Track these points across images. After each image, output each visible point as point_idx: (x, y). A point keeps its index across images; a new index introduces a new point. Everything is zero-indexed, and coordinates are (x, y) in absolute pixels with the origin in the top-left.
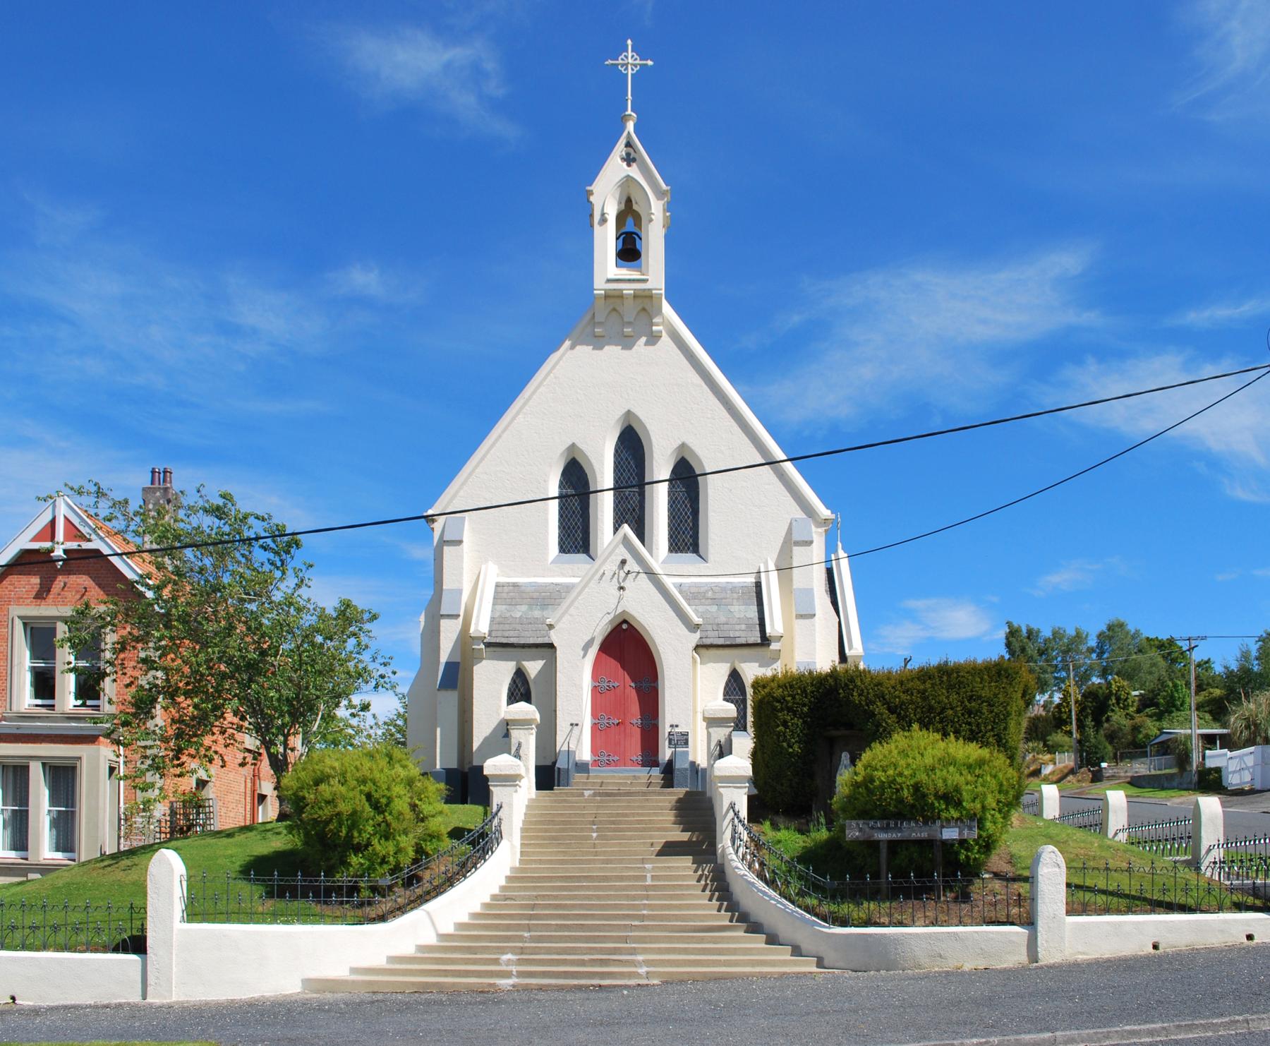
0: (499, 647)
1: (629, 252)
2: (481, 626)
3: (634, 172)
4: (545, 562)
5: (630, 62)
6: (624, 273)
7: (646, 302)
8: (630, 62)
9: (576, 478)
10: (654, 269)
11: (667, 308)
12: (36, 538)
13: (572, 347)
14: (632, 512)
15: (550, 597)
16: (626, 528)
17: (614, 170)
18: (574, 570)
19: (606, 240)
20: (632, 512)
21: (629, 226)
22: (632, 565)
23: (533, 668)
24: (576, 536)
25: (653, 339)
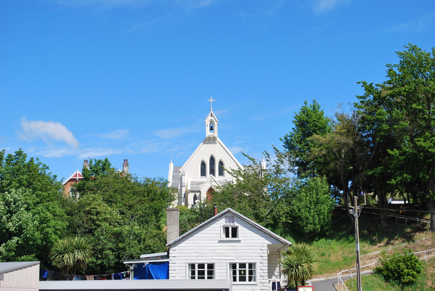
0: (192, 191)
1: (212, 129)
2: (189, 188)
3: (212, 118)
4: (198, 178)
5: (211, 100)
6: (212, 134)
7: (214, 139)
8: (211, 100)
9: (203, 164)
10: (215, 133)
11: (218, 139)
12: (73, 177)
13: (203, 144)
14: (212, 172)
15: (200, 183)
16: (211, 175)
17: (209, 118)
18: (203, 179)
19: (208, 128)
20: (212, 172)
21: (212, 125)
22: (212, 180)
23: (198, 194)
24: (203, 173)
25: (216, 143)
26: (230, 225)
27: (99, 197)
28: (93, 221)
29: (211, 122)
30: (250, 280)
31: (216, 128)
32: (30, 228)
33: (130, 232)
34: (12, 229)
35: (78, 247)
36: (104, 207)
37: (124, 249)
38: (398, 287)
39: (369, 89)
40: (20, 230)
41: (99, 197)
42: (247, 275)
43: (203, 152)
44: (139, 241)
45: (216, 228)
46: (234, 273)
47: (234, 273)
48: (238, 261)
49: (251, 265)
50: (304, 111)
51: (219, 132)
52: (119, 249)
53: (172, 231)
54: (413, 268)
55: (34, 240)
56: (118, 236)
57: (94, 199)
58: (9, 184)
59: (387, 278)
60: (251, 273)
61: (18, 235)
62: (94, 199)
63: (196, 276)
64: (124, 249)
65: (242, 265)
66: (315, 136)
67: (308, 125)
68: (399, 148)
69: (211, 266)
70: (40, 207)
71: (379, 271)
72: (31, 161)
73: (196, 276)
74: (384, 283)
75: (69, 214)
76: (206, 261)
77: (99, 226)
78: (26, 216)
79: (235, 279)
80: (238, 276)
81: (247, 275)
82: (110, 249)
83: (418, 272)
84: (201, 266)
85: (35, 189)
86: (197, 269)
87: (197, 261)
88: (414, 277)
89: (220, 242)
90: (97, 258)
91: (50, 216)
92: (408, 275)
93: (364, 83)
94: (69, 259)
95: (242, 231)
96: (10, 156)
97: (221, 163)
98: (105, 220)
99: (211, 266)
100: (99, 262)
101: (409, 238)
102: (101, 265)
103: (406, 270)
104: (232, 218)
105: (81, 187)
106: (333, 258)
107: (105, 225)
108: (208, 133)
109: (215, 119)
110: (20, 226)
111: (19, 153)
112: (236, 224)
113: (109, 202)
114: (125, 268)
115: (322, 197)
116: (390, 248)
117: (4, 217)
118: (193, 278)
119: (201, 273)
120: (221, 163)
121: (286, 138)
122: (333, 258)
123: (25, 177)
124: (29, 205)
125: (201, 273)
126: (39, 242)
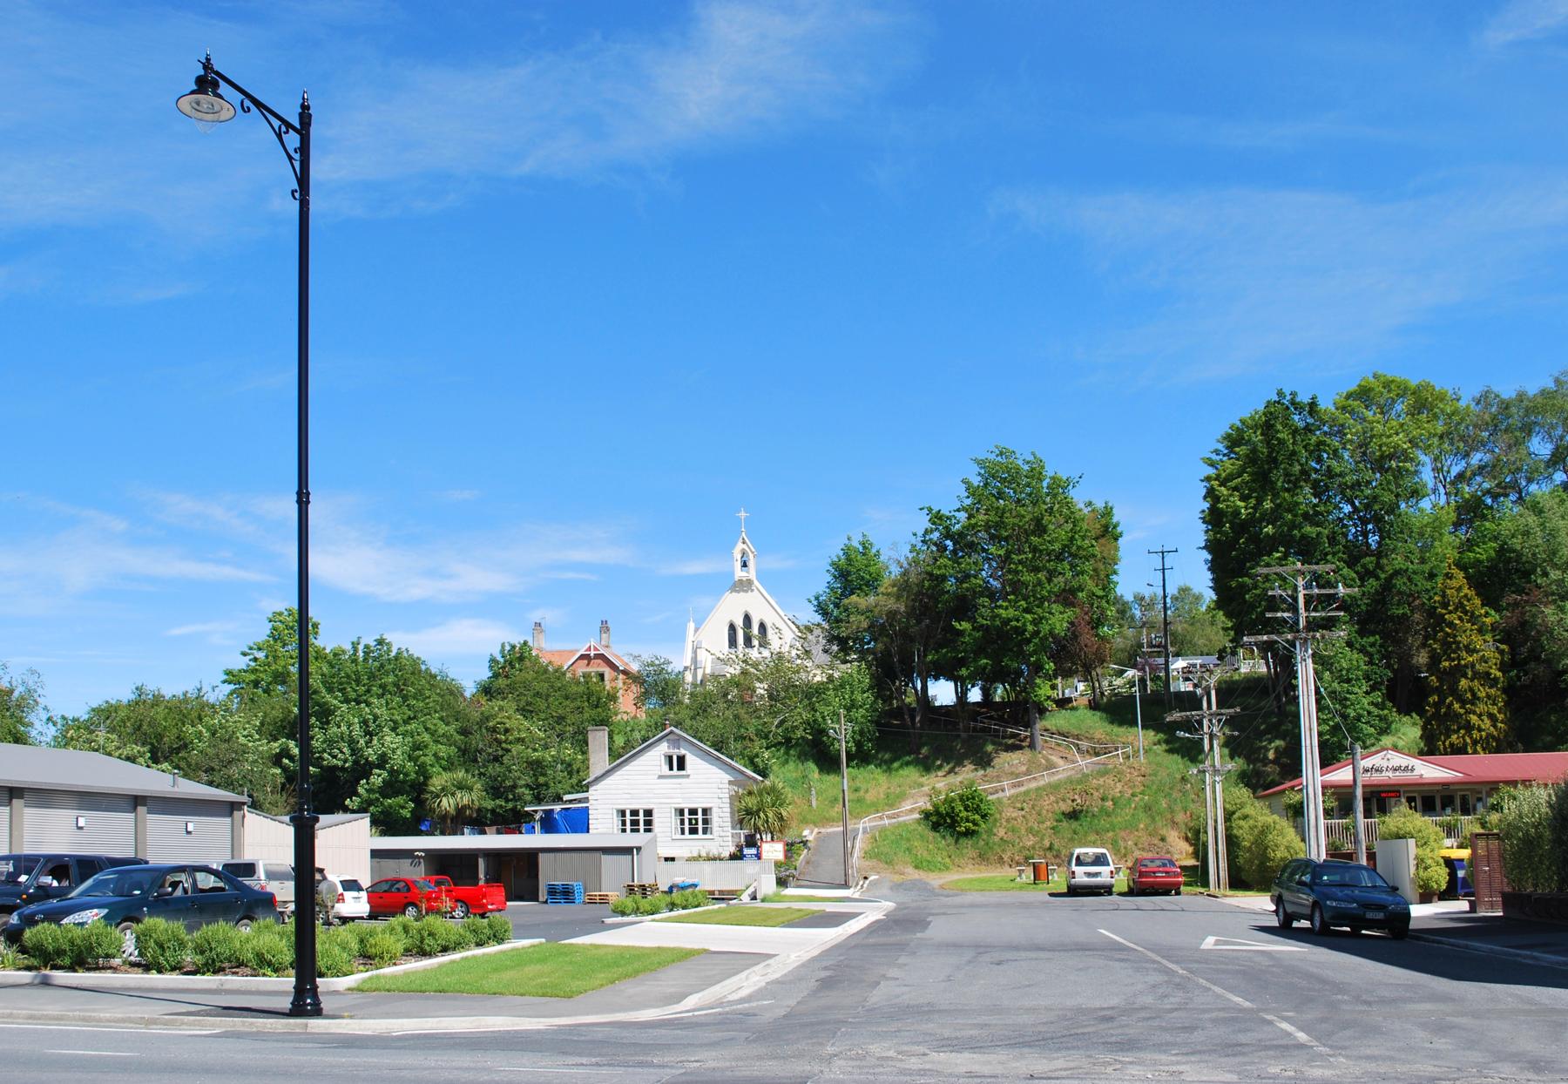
1: (745, 565)
5: (743, 514)
8: (743, 514)
9: (732, 628)
17: (740, 546)
19: (738, 564)
24: (733, 642)
26: (675, 752)
27: (510, 705)
28: (499, 742)
29: (744, 553)
30: (705, 831)
31: (751, 564)
32: (398, 759)
33: (556, 760)
34: (373, 758)
35: (461, 786)
36: (517, 722)
37: (546, 785)
38: (950, 840)
39: (937, 518)
40: (383, 761)
41: (510, 705)
42: (700, 826)
43: (732, 608)
44: (570, 774)
45: (655, 757)
46: (682, 822)
47: (682, 822)
48: (687, 806)
49: (705, 811)
50: (847, 551)
51: (757, 572)
52: (539, 786)
53: (599, 759)
54: (977, 810)
55: (406, 775)
56: (536, 766)
57: (501, 709)
58: (368, 691)
59: (935, 827)
60: (706, 822)
61: (381, 766)
62: (501, 709)
63: (628, 827)
64: (546, 785)
65: (693, 812)
66: (854, 598)
67: (852, 575)
68: (972, 620)
69: (648, 813)
70: (412, 726)
71: (927, 815)
72: (399, 653)
73: (628, 827)
74: (931, 835)
75: (464, 732)
76: (641, 806)
77: (508, 751)
78: (391, 740)
79: (683, 833)
80: (687, 826)
81: (700, 826)
82: (527, 786)
83: (984, 816)
84: (635, 813)
85: (405, 698)
86: (628, 818)
87: (629, 806)
88: (975, 824)
89: (661, 777)
90: (507, 800)
91: (427, 737)
92: (968, 820)
93: (930, 510)
94: (447, 804)
95: (691, 760)
96: (367, 646)
97: (762, 626)
98: (520, 740)
99: (648, 813)
100: (510, 805)
101: (984, 762)
102: (514, 810)
103: (964, 814)
104: (677, 742)
105: (487, 690)
106: (869, 797)
107: (516, 749)
108: (739, 574)
109: (750, 548)
110: (384, 755)
111: (380, 642)
112: (683, 752)
113: (526, 712)
114: (529, 816)
115: (859, 698)
116: (952, 779)
117: (362, 741)
118: (624, 831)
119: (635, 823)
120: (762, 626)
121: (817, 598)
122: (869, 797)
123: (391, 679)
124: (395, 722)
125: (635, 823)
126: (413, 776)
